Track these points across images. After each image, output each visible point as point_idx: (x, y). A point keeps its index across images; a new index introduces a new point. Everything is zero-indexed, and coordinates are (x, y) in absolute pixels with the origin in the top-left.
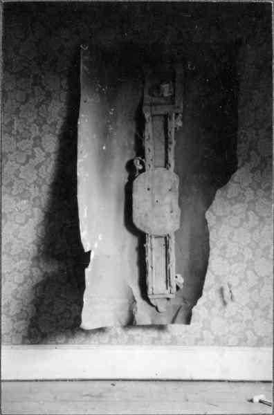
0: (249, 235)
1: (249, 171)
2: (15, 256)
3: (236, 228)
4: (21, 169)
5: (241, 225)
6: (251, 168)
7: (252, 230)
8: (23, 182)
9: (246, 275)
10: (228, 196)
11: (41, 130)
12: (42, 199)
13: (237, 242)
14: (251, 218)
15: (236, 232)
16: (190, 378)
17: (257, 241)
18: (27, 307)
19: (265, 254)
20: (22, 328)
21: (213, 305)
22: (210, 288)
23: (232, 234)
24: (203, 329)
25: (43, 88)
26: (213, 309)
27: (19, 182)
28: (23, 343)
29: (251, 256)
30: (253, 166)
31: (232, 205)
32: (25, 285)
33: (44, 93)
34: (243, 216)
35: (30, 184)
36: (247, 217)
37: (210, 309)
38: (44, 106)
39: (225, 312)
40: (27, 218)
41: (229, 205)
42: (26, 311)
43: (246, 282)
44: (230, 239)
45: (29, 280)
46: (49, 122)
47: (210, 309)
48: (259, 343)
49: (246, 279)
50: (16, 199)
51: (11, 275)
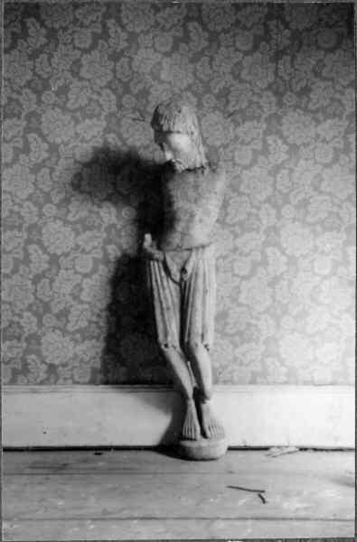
0: (272, 66)
2: (76, 223)
3: (327, 166)
4: (325, 176)
7: (277, 56)
8: (327, 197)
9: (27, 143)
10: (311, 106)
11: (39, 102)
13: (330, 194)
14: (31, 31)
15: (327, 173)
16: (242, 445)
17: (47, 300)
18: (99, 316)
19: (60, 101)
20: (92, 353)
21: (48, 199)
23: (319, 178)
24: (29, 242)
26: (285, 319)
28: (93, 382)
31: (318, 122)
32: (96, 276)
33: (44, 31)
35: (342, 202)
37: (40, 207)
38: (44, 57)
39: (68, 211)
40: (336, 265)
41: (314, 123)
42: (97, 323)
44: (316, 189)
45: (101, 267)
47: (40, 207)
50: (314, 231)
51: (69, 258)
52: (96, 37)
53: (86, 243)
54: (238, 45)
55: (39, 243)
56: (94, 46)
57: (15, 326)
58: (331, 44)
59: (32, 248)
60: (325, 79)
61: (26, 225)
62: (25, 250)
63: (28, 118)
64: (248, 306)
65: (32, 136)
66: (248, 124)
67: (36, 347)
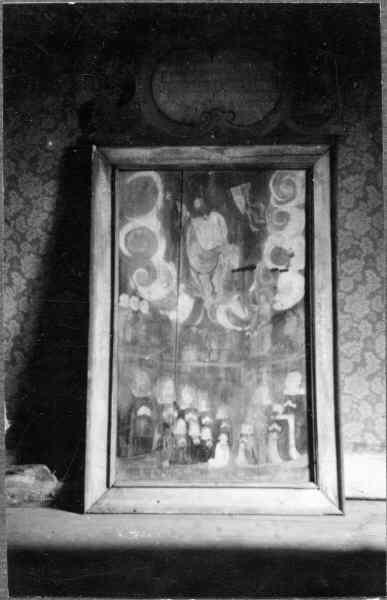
1: (365, 214)
5: (357, 206)
6: (368, 293)
9: (363, 359)
11: (19, 250)
12: (25, 340)
14: (369, 279)
22: (323, 288)
25: (21, 194)
27: (47, 155)
29: (370, 333)
30: (370, 290)
33: (21, 200)
34: (359, 277)
36: (364, 277)
38: (22, 218)
43: (366, 201)
46: (30, 239)
47: (18, 244)
48: (380, 451)
49: (363, 363)
52: (357, 283)
53: (348, 350)
54: (351, 121)
55: (19, 271)
56: (355, 289)
57: (354, 330)
58: (349, 371)
59: (367, 355)
60: (348, 146)
61: (363, 337)
62: (362, 356)
63: (365, 341)
64: (351, 314)
65: (368, 273)
66: (352, 178)
67: (373, 264)
